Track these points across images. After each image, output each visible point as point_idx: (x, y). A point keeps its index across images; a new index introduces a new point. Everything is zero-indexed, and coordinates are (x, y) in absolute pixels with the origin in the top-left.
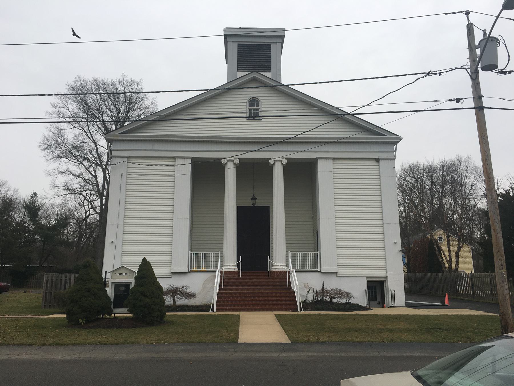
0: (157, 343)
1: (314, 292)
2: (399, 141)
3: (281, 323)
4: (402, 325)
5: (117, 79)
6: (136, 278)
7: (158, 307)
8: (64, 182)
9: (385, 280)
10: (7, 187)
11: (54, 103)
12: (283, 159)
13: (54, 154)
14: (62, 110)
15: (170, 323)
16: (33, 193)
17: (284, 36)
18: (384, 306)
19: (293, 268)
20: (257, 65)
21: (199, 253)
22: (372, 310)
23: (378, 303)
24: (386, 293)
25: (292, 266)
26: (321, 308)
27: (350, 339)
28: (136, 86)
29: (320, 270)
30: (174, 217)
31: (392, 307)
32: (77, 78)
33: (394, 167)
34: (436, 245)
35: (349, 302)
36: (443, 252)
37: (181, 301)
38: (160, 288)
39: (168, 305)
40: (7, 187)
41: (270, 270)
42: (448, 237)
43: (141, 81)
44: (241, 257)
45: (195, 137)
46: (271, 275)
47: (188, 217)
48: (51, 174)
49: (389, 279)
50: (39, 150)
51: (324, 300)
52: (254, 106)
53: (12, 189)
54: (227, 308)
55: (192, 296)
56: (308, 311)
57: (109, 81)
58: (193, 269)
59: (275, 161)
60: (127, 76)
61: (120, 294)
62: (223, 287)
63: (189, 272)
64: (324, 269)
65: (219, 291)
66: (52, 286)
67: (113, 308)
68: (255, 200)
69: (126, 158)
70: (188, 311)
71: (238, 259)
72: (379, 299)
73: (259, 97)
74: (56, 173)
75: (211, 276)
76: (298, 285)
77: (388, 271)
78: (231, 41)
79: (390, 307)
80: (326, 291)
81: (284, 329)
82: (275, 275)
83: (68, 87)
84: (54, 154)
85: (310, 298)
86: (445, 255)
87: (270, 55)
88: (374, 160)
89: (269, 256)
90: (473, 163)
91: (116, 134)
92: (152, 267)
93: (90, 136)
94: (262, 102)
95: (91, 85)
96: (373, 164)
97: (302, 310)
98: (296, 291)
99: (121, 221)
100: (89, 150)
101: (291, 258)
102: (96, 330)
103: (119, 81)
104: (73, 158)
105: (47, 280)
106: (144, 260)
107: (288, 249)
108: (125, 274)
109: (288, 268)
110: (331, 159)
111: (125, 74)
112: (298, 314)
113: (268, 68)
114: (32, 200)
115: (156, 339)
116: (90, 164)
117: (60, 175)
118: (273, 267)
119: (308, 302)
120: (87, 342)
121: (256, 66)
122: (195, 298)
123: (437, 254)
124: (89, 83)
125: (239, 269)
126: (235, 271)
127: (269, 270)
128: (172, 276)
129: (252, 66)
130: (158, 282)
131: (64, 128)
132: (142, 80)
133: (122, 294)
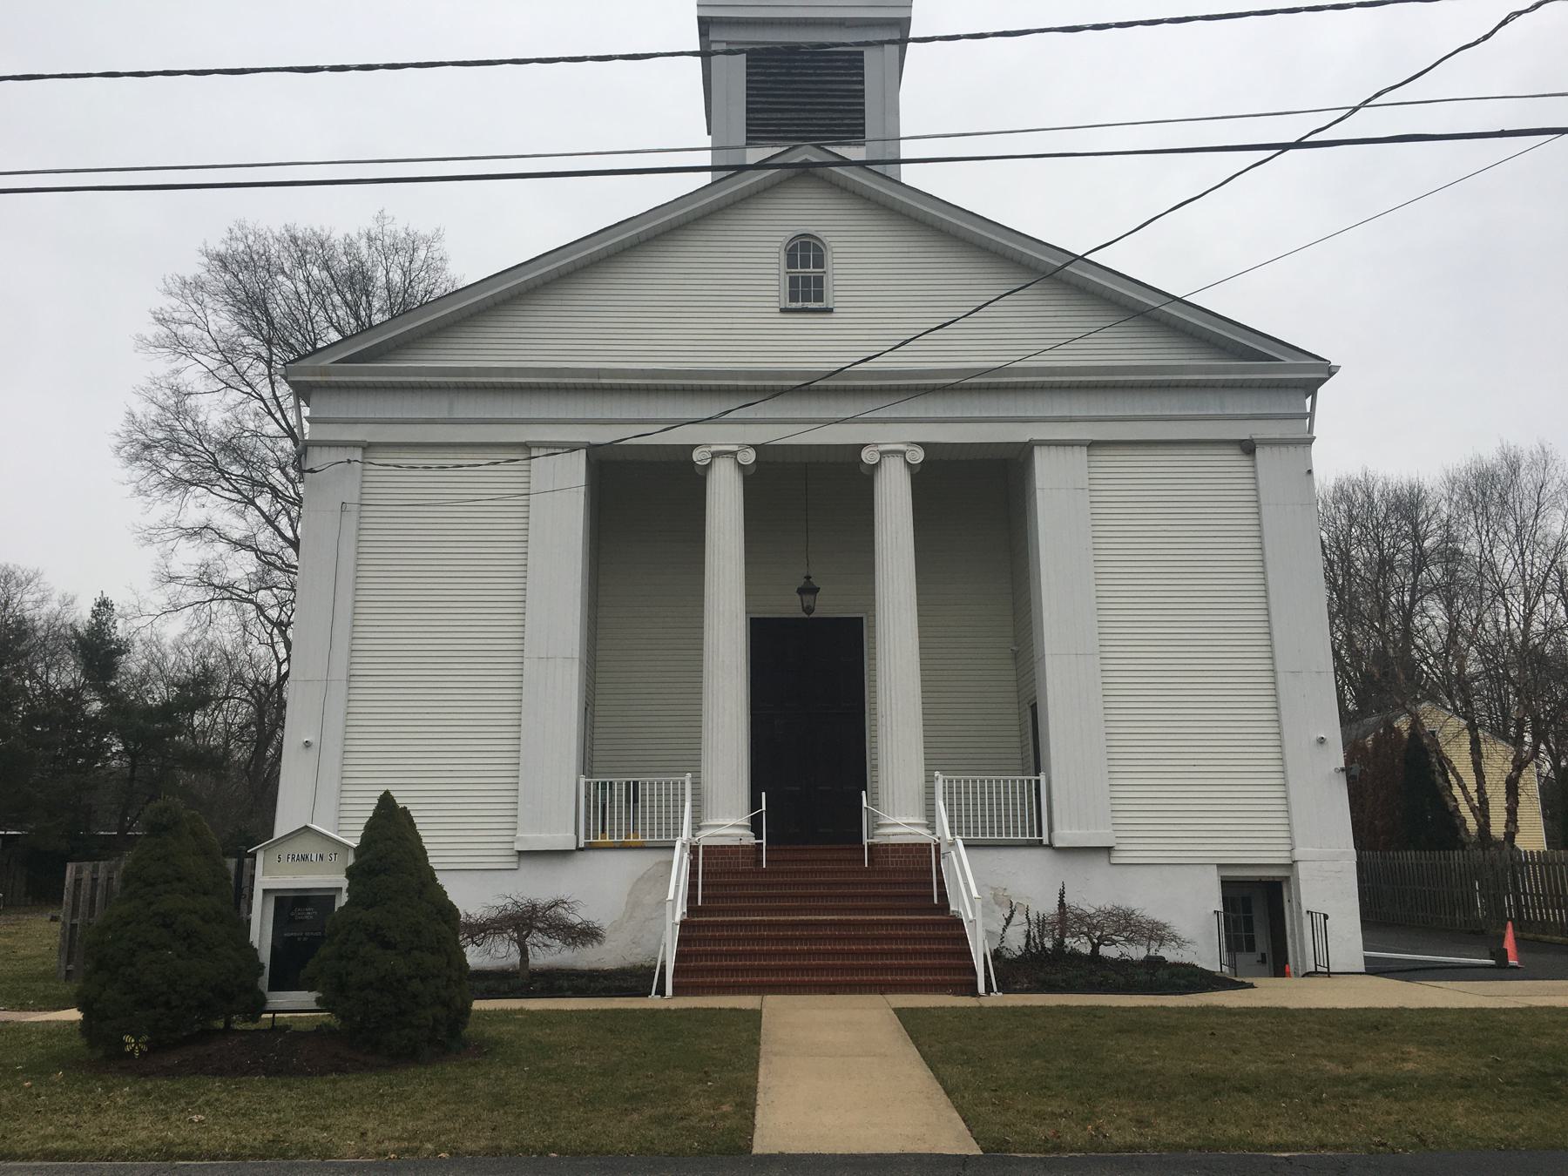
0: (407, 1150)
1: (1028, 919)
2: (1326, 380)
3: (926, 1048)
4: (1417, 1062)
5: (362, 232)
6: (350, 873)
7: (437, 988)
8: (199, 564)
9: (1287, 878)
10: (40, 591)
11: (161, 309)
12: (910, 448)
13: (164, 472)
14: (187, 330)
15: (484, 1050)
16: (98, 600)
17: (909, 19)
18: (1287, 970)
19: (952, 834)
20: (815, 121)
21: (620, 782)
22: (1251, 986)
23: (1260, 959)
24: (1292, 925)
25: (950, 828)
26: (1063, 980)
27: (1234, 1132)
28: (422, 254)
29: (1050, 841)
30: (526, 654)
31: (1316, 972)
32: (236, 230)
33: (1310, 472)
34: (1434, 755)
35: (1159, 954)
36: (1459, 779)
37: (549, 954)
38: (451, 910)
39: (505, 968)
40: (40, 591)
41: (870, 841)
42: (1472, 729)
43: (438, 235)
44: (764, 794)
45: (598, 373)
46: (873, 861)
47: (577, 655)
48: (156, 540)
49: (1302, 869)
50: (119, 462)
51: (1067, 950)
52: (805, 265)
53: (56, 596)
54: (716, 980)
55: (587, 934)
56: (1015, 992)
57: (337, 237)
58: (628, 836)
59: (882, 453)
60: (394, 219)
61: (295, 934)
62: (700, 904)
63: (579, 849)
64: (1066, 833)
65: (685, 917)
66: (92, 901)
67: (269, 990)
68: (812, 597)
69: (359, 447)
70: (570, 993)
71: (755, 803)
72: (1262, 944)
73: (824, 234)
74: (171, 535)
75: (660, 862)
76: (977, 896)
77: (1298, 842)
78: (723, 42)
79: (1308, 974)
80: (1077, 916)
81: (942, 1081)
82: (887, 857)
83: (206, 260)
84: (164, 472)
85: (1016, 941)
86: (1463, 788)
87: (860, 87)
88: (1238, 447)
89: (864, 792)
90: (1560, 470)
91: (321, 364)
92: (421, 833)
93: (278, 415)
94: (835, 250)
95: (276, 246)
96: (1233, 461)
97: (995, 989)
98: (971, 917)
99: (340, 672)
100: (278, 461)
101: (944, 799)
102: (177, 1086)
103: (370, 239)
104: (226, 485)
105: (76, 880)
106: (386, 800)
107: (933, 767)
108: (314, 860)
109: (934, 834)
110: (1081, 446)
111: (386, 213)
112: (981, 1008)
113: (854, 132)
114: (99, 623)
115: (405, 1129)
116: (279, 505)
117: (183, 540)
118: (882, 831)
119: (1008, 956)
120: (118, 1142)
121: (811, 125)
122: (600, 943)
123: (1441, 786)
124: (271, 241)
125: (758, 836)
126: (743, 846)
127: (866, 841)
128: (519, 862)
129: (797, 125)
130: (441, 887)
131: (194, 391)
132: (441, 233)
133: (304, 936)
